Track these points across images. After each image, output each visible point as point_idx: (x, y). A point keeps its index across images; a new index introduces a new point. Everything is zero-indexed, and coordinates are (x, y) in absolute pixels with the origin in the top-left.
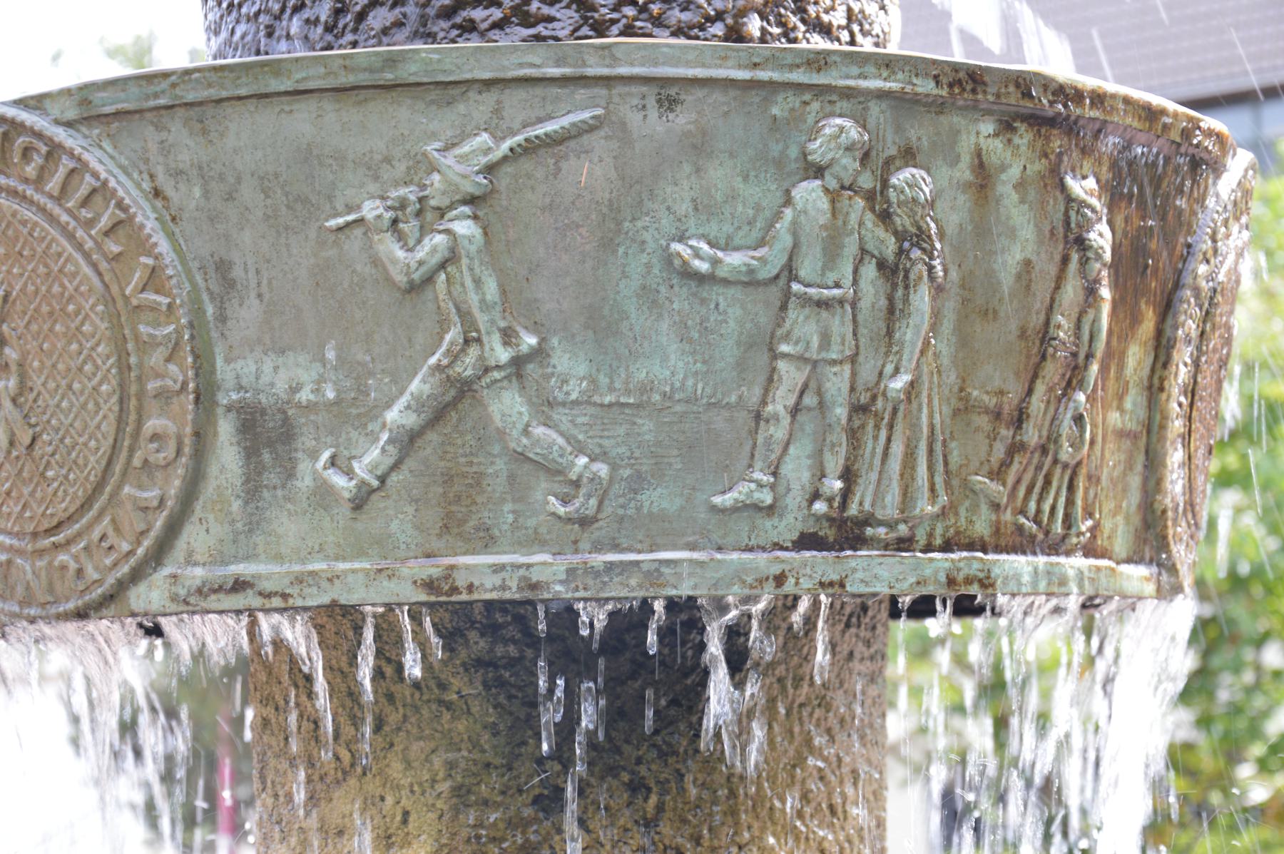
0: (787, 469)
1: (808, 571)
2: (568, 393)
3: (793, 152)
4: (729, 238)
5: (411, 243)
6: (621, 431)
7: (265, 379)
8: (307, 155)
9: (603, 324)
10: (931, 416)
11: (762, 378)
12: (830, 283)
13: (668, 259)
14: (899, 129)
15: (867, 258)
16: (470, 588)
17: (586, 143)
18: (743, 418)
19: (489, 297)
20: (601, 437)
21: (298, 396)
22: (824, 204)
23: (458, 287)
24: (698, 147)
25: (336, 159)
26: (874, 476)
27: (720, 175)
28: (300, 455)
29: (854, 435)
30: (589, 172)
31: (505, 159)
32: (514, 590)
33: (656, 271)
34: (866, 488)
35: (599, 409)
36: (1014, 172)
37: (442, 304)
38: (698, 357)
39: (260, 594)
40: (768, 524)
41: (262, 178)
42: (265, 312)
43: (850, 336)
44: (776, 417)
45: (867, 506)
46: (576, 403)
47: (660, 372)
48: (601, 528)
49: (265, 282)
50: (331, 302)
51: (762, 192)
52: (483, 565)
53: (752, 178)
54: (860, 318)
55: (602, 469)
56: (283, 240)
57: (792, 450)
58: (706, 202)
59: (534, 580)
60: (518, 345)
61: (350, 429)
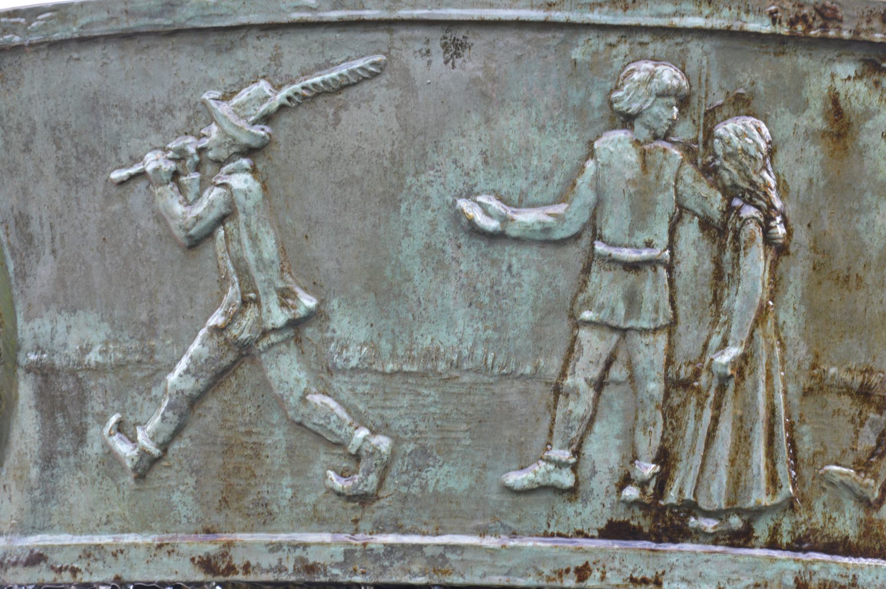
0: (592, 448)
1: (617, 564)
2: (347, 360)
3: (596, 99)
4: (523, 194)
5: (191, 197)
6: (405, 401)
7: (59, 339)
8: (95, 104)
9: (385, 286)
10: (771, 395)
14: (726, 73)
15: (687, 217)
16: (247, 568)
17: (366, 91)
18: (540, 392)
19: (266, 255)
20: (383, 408)
21: (88, 357)
22: (632, 157)
23: (235, 244)
24: (486, 96)
25: (121, 109)
26: (697, 461)
27: (512, 126)
28: (90, 420)
30: (368, 121)
31: (282, 107)
32: (291, 570)
33: (441, 229)
34: (687, 474)
35: (380, 377)
37: (221, 262)
38: (489, 323)
39: (52, 568)
40: (570, 510)
41: (54, 129)
42: (59, 269)
43: (665, 303)
44: (576, 391)
45: (688, 495)
47: (446, 340)
48: (382, 507)
49: (58, 237)
50: (117, 258)
51: (561, 145)
52: (260, 544)
54: (679, 283)
55: (383, 443)
56: (73, 194)
57: (597, 427)
58: (496, 155)
59: (311, 561)
60: (294, 307)
61: (135, 394)
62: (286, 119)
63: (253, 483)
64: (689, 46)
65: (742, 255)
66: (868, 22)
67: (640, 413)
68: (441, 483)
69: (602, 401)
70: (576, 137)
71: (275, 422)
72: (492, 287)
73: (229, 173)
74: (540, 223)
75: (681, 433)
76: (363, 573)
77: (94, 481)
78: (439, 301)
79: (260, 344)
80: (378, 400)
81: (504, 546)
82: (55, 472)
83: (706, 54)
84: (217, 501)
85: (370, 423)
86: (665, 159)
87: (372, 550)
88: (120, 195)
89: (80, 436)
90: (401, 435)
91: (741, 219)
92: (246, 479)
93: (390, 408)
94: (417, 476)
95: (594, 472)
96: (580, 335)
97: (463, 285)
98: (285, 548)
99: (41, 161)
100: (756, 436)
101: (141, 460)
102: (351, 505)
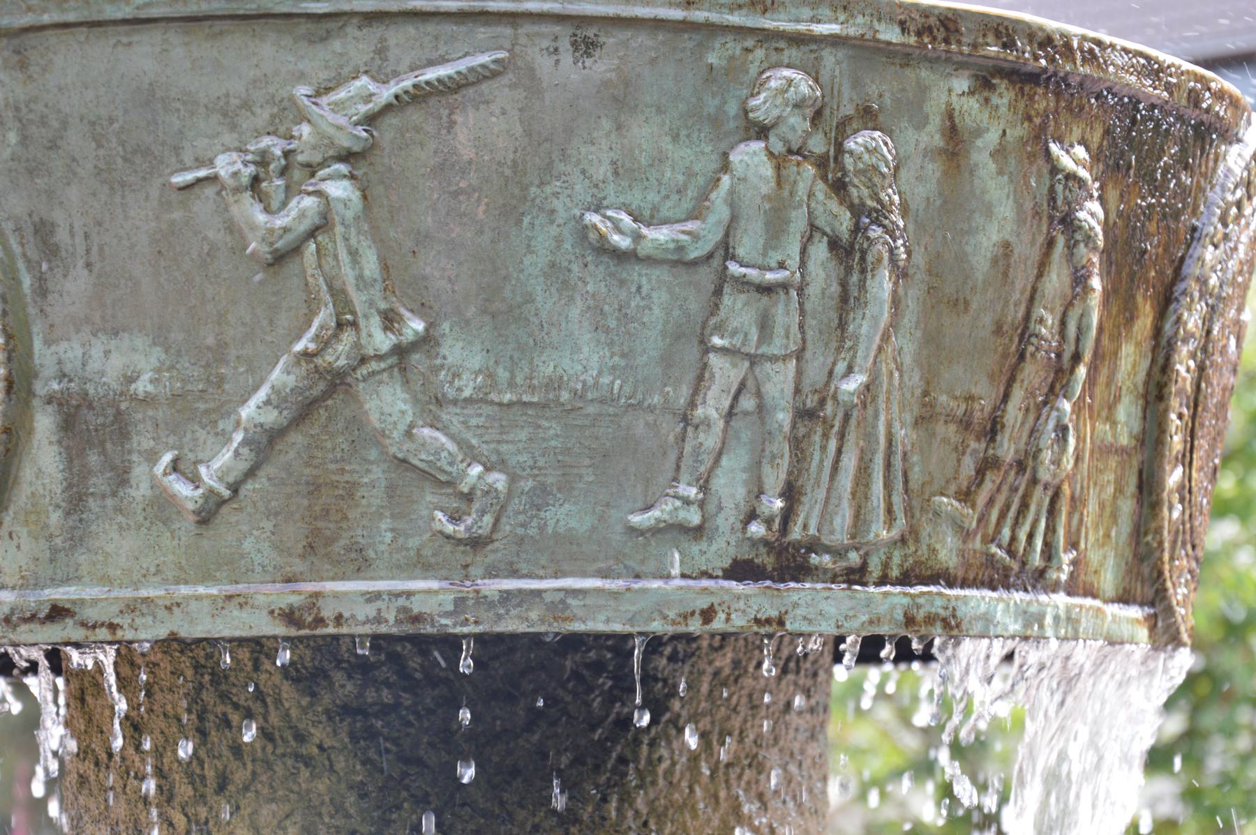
0: (719, 482)
2: (460, 389)
3: (732, 108)
4: (655, 209)
5: (275, 204)
6: (523, 435)
8: (149, 98)
11: (691, 376)
12: (773, 264)
13: (583, 231)
14: (857, 84)
15: (817, 236)
16: (339, 619)
19: (367, 273)
21: (133, 386)
22: (768, 170)
23: (330, 259)
24: (620, 99)
25: (184, 103)
26: (821, 494)
27: (645, 133)
28: (135, 457)
29: (798, 445)
32: (392, 620)
33: (567, 246)
34: (811, 508)
35: (496, 408)
36: (992, 137)
37: (310, 280)
41: (93, 124)
43: (795, 329)
44: (707, 423)
45: (812, 531)
46: (469, 401)
48: (495, 551)
50: (176, 274)
51: (695, 155)
52: (355, 592)
53: (682, 138)
54: (808, 306)
55: (499, 480)
56: (118, 199)
57: (725, 461)
58: (628, 165)
59: (416, 611)
61: (197, 427)
62: (392, 120)
63: (345, 526)
64: (823, 53)
65: (869, 276)
66: (984, 35)
67: (767, 443)
68: (562, 523)
69: (731, 433)
70: (710, 148)
71: (372, 458)
72: (620, 310)
73: (324, 180)
74: (673, 241)
75: (805, 465)
76: (476, 622)
77: (139, 527)
78: (564, 325)
79: (359, 372)
80: (493, 434)
81: (628, 589)
82: (84, 516)
83: (838, 63)
84: (300, 546)
85: (484, 459)
86: (799, 173)
87: (486, 597)
88: (181, 202)
89: (122, 478)
90: (519, 472)
91: (868, 238)
92: (336, 522)
93: (507, 442)
94: (536, 516)
95: (720, 508)
96: (711, 362)
97: (589, 308)
98: (385, 597)
99: (74, 160)
100: (876, 467)
101: (206, 502)
102: (462, 548)
